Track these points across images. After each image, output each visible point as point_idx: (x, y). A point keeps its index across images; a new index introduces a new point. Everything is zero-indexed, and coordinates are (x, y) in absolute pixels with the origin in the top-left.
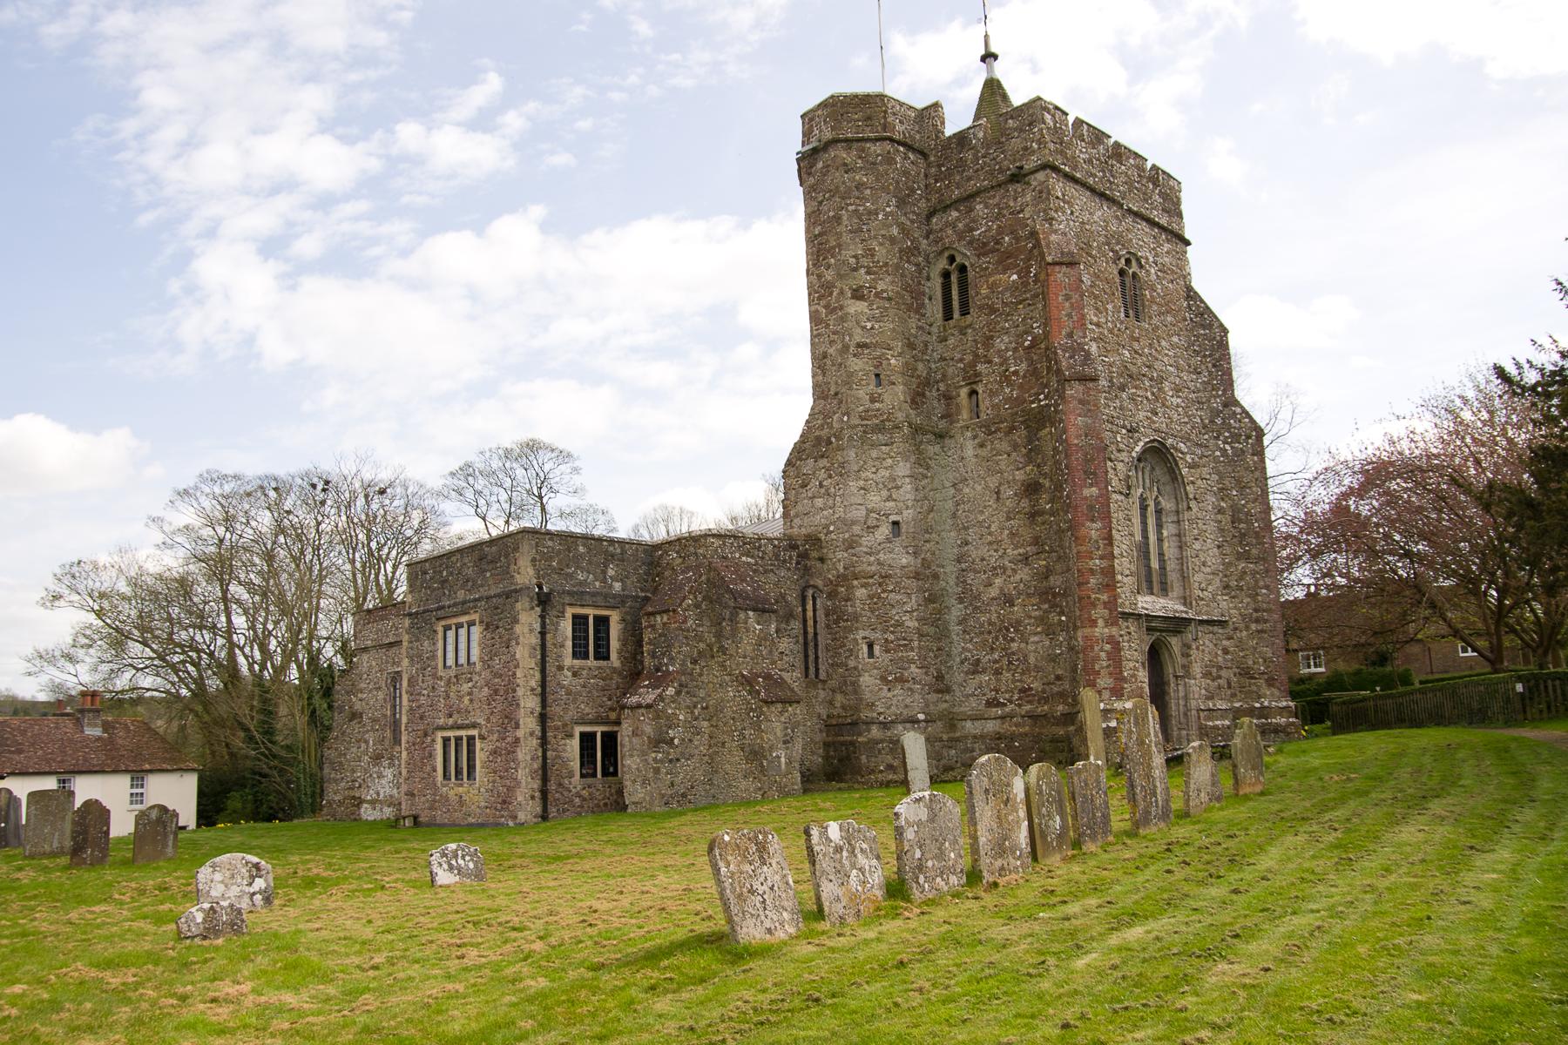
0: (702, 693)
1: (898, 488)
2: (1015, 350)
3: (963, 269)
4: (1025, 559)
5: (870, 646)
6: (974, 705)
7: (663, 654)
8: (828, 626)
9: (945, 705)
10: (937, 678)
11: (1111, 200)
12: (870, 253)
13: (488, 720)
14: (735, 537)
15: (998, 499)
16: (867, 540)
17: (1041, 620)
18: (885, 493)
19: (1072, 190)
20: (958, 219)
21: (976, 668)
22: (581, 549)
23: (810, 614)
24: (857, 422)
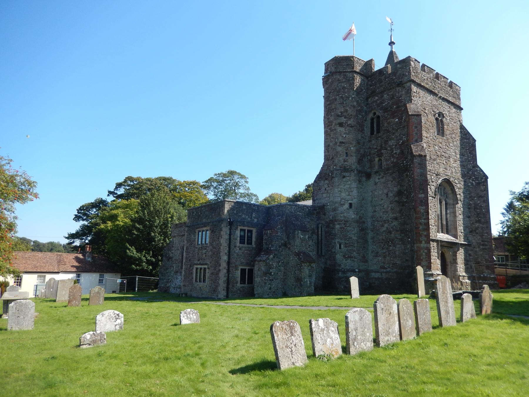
0: (282, 258)
1: (352, 191)
2: (396, 145)
4: (396, 219)
7: (270, 244)
8: (326, 237)
9: (365, 267)
11: (435, 94)
12: (346, 111)
15: (387, 197)
17: (401, 240)
20: (378, 100)
21: (377, 255)
22: (244, 207)
23: (320, 233)
24: (339, 168)
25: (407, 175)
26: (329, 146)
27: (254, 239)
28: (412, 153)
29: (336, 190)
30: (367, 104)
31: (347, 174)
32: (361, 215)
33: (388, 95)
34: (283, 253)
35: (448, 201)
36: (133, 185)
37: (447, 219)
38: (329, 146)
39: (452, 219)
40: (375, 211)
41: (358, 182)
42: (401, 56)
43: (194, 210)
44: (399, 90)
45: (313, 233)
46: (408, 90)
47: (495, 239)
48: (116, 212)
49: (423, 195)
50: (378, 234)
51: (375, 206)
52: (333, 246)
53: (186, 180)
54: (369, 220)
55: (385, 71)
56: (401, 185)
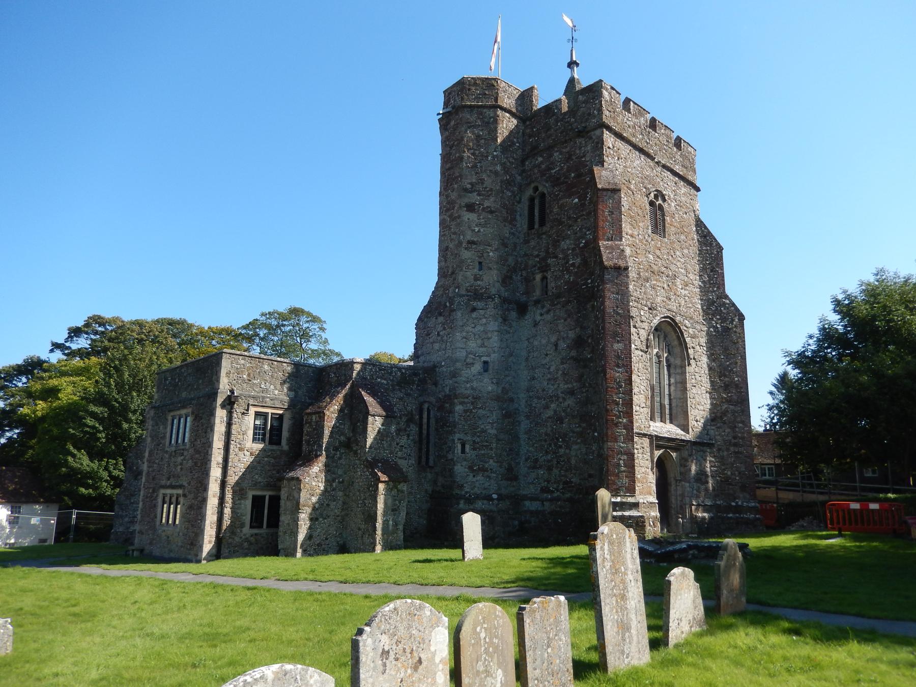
0: (340, 472)
1: (489, 339)
2: (573, 249)
3: (543, 196)
4: (571, 392)
6: (531, 490)
7: (315, 443)
8: (437, 429)
9: (512, 489)
11: (648, 155)
12: (482, 181)
13: (189, 484)
14: (374, 365)
15: (556, 349)
18: (479, 342)
19: (620, 144)
20: (542, 163)
21: (535, 465)
22: (266, 367)
23: (425, 421)
24: (464, 292)
25: (593, 306)
26: (447, 248)
27: (285, 434)
28: (602, 262)
30: (523, 171)
31: (480, 304)
32: (507, 386)
33: (561, 153)
34: (342, 461)
35: (672, 360)
36: (103, 333)
37: (670, 395)
38: (447, 248)
40: (533, 378)
41: (500, 320)
42: (585, 79)
43: (168, 374)
44: (581, 143)
45: (410, 420)
46: (598, 143)
47: (758, 435)
48: (56, 383)
51: (533, 368)
52: (450, 447)
53: (213, 325)
54: (522, 395)
55: (557, 107)
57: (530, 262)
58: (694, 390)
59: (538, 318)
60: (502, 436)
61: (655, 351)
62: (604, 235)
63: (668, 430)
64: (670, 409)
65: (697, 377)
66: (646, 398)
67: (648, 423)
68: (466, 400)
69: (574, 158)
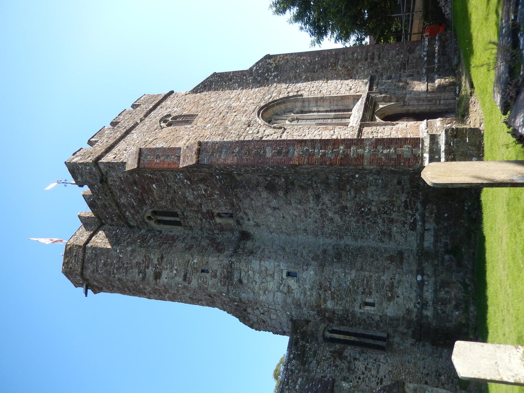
1: (267, 269)
2: (193, 190)
3: (155, 213)
4: (317, 197)
5: (367, 304)
6: (413, 241)
8: (351, 326)
9: (411, 257)
10: (392, 261)
12: (138, 264)
15: (278, 209)
16: (297, 294)
17: (357, 190)
19: (115, 150)
20: (130, 212)
23: (341, 337)
29: (262, 298)
30: (138, 227)
31: (236, 275)
35: (297, 109)
37: (327, 111)
38: (191, 298)
39: (326, 103)
40: (305, 230)
41: (251, 257)
44: (111, 181)
45: (339, 354)
46: (109, 167)
49: (268, 149)
50: (347, 229)
51: (296, 230)
52: (368, 317)
54: (321, 241)
56: (258, 186)
57: (207, 226)
58: (324, 92)
59: (252, 223)
60: (358, 265)
61: (287, 122)
62: (175, 163)
63: (357, 112)
64: (339, 111)
65: (313, 89)
66: (326, 129)
67: (350, 128)
68: (322, 296)
69: (123, 187)
